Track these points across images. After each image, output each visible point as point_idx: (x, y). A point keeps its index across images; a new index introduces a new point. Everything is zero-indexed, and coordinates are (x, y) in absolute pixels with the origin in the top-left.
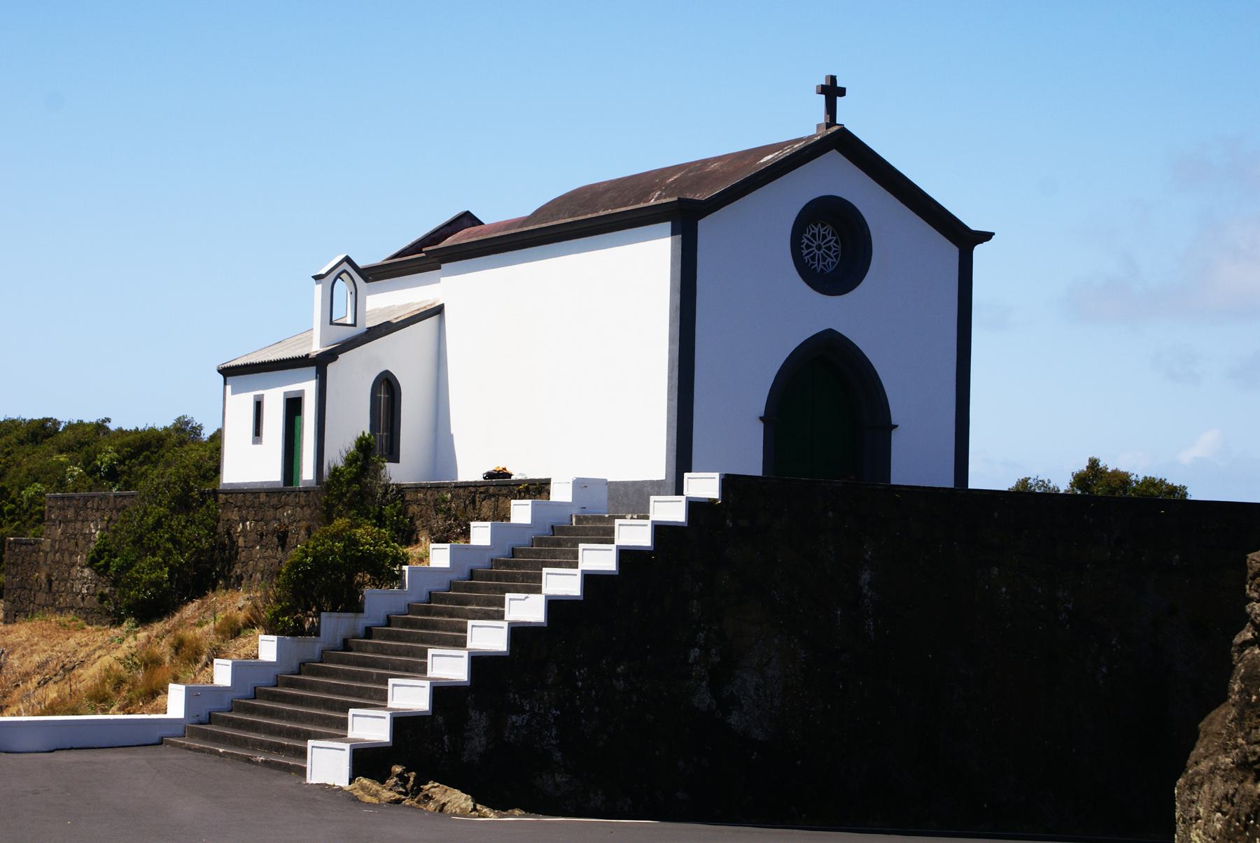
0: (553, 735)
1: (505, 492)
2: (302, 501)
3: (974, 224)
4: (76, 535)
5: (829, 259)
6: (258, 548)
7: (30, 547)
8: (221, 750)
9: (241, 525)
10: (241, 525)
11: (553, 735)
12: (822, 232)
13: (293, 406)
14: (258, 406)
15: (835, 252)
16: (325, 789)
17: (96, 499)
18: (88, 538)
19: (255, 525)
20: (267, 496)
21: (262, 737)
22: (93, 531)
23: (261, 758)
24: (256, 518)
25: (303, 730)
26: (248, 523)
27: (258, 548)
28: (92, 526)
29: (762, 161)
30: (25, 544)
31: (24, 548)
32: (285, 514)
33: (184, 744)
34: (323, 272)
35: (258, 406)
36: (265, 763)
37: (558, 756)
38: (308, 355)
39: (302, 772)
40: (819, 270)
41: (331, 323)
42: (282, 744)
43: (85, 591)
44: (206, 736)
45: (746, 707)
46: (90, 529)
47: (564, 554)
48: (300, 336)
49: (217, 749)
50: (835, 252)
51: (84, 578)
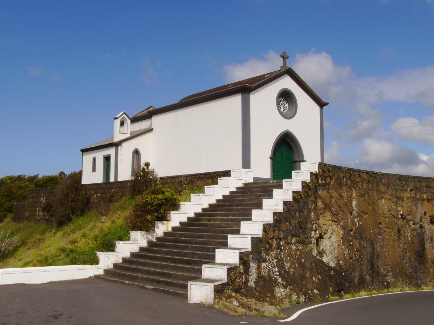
0: (277, 271)
1: (208, 177)
2: (119, 186)
3: (324, 100)
4: (36, 201)
5: (285, 108)
6: (102, 202)
7: (21, 206)
8: (127, 282)
9: (95, 195)
10: (95, 195)
11: (277, 271)
12: (282, 100)
13: (107, 159)
14: (94, 160)
15: (286, 106)
16: (200, 306)
17: (43, 190)
18: (41, 202)
19: (101, 195)
20: (105, 185)
21: (145, 276)
22: (42, 200)
23: (151, 287)
24: (101, 193)
25: (167, 273)
26: (98, 194)
27: (102, 202)
28: (42, 198)
29: (265, 77)
30: (20, 205)
31: (20, 206)
32: (113, 191)
33: (106, 278)
34: (117, 117)
35: (94, 160)
36: (154, 289)
37: (280, 280)
38: (112, 143)
39: (185, 297)
40: (282, 111)
41: (120, 133)
42: (159, 280)
43: (40, 218)
44: (119, 275)
45: (328, 254)
46: (41, 199)
47: (250, 196)
48: (109, 139)
49: (124, 281)
50: (286, 106)
51: (39, 214)
